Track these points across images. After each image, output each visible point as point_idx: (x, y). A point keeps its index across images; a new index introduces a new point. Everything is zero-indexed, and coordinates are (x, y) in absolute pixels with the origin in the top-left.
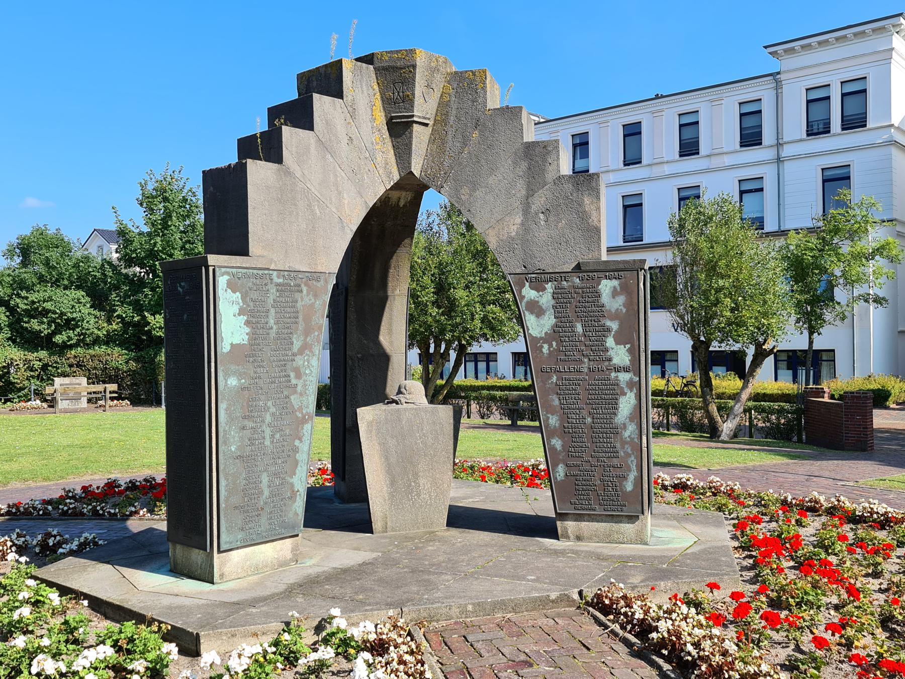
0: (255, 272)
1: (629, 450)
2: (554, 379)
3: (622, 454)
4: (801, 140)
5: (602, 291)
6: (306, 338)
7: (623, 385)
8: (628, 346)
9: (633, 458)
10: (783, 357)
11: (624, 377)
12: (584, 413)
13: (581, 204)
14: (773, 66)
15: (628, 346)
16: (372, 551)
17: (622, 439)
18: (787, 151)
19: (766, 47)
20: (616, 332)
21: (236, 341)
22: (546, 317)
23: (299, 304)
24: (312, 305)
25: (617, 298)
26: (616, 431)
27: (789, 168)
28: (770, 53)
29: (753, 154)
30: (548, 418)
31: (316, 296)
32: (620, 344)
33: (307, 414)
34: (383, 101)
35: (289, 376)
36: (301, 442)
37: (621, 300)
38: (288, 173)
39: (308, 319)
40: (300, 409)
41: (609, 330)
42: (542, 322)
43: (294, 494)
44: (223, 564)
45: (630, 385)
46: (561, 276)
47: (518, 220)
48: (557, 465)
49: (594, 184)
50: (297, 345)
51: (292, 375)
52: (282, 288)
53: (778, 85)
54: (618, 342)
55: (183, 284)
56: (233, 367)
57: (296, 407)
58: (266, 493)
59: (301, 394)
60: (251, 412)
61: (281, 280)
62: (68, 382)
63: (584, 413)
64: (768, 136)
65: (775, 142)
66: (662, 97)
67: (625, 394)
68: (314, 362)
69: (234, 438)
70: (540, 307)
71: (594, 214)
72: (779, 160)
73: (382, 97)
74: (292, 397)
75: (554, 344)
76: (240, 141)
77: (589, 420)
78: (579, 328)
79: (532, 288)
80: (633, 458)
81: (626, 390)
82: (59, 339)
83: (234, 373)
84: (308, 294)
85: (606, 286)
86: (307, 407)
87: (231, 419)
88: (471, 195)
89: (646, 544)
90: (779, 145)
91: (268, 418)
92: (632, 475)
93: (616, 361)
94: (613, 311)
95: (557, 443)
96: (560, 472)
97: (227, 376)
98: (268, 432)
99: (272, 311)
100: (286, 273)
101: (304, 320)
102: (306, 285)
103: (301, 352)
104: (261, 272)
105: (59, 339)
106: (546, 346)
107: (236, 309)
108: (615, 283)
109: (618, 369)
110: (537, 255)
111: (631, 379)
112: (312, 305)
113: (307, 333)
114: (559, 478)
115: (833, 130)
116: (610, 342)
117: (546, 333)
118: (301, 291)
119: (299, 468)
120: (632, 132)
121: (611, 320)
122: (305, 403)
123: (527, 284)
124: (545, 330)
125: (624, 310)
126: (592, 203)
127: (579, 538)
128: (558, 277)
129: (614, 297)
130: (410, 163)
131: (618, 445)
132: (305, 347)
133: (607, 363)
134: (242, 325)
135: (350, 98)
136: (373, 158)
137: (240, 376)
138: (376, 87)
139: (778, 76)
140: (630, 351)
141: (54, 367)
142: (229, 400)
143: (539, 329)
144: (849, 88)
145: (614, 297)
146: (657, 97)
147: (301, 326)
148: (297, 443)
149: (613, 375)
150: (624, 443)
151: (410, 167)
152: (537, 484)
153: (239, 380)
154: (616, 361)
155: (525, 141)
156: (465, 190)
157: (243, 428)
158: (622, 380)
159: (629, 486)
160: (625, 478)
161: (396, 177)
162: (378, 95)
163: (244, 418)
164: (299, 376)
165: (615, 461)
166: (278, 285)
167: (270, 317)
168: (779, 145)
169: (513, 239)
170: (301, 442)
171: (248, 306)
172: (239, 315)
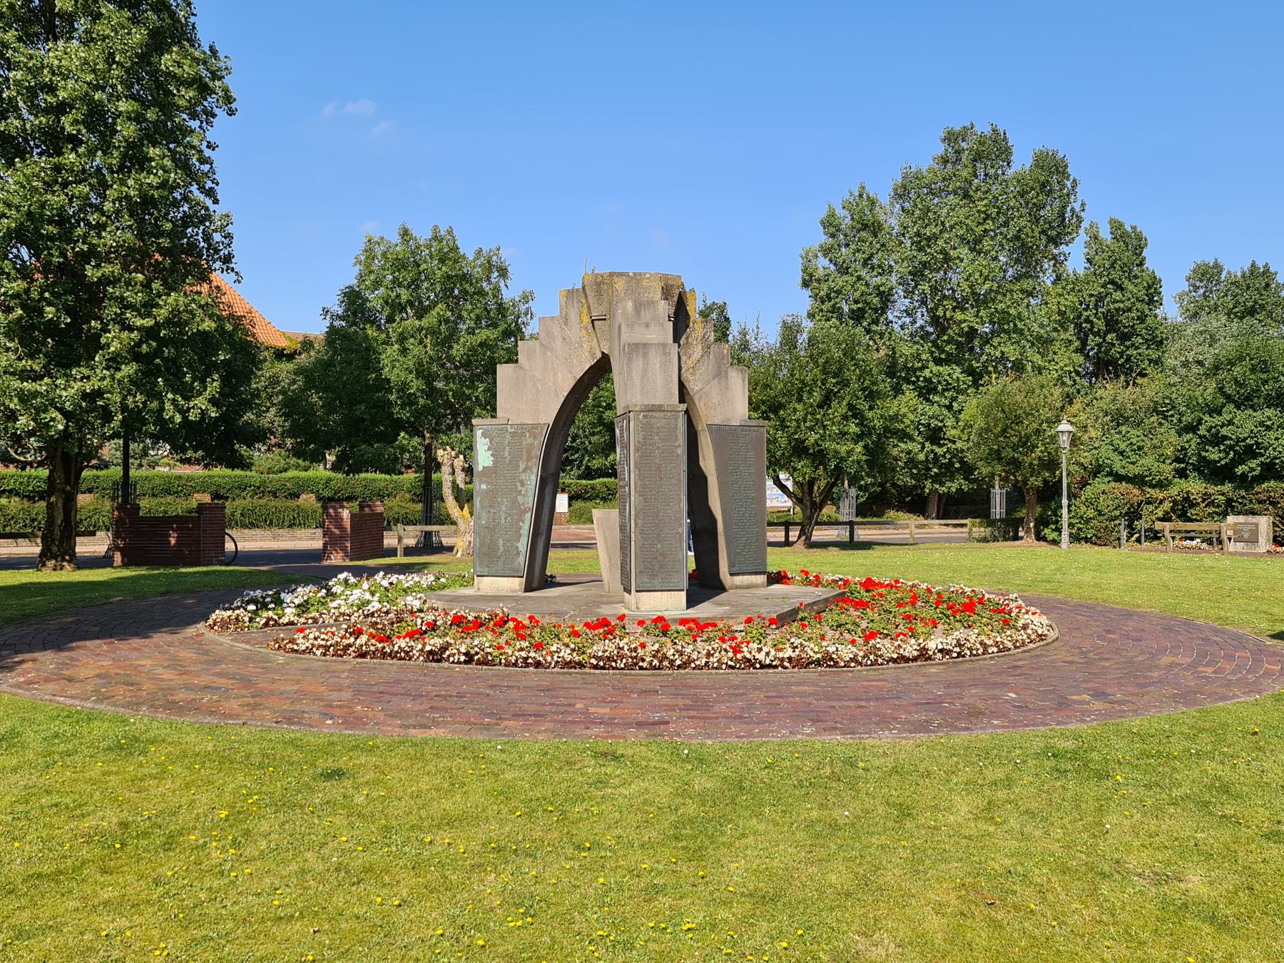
31: (535, 438)
38: (521, 368)
39: (529, 452)
40: (523, 504)
43: (518, 553)
44: (479, 583)
50: (522, 467)
52: (513, 435)
62: (1242, 521)
68: (533, 477)
82: (1240, 470)
83: (485, 482)
87: (482, 507)
91: (504, 508)
97: (480, 483)
98: (503, 516)
103: (524, 471)
105: (1240, 470)
107: (486, 447)
113: (528, 459)
137: (488, 484)
141: (1240, 503)
152: (1046, 607)
164: (523, 485)
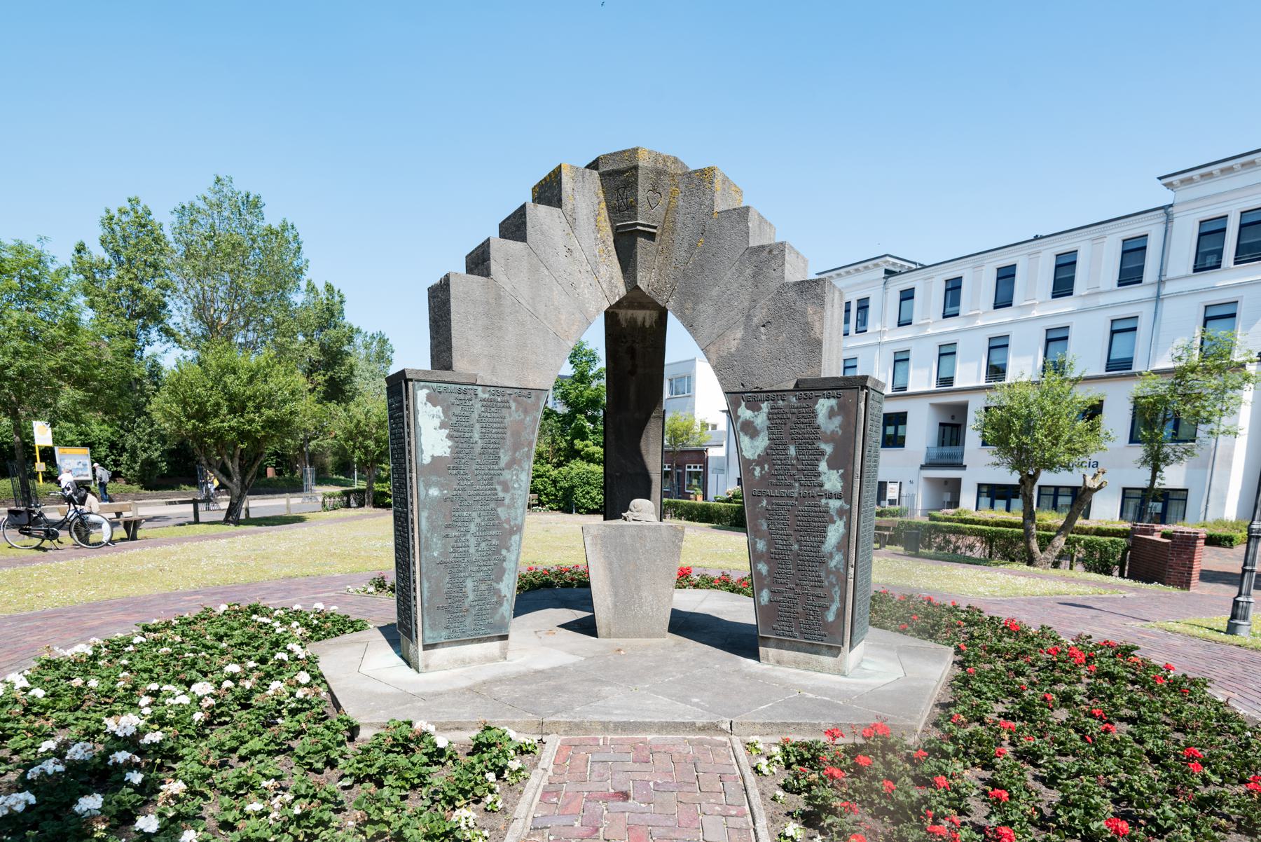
0: (458, 386)
1: (834, 581)
2: (764, 503)
3: (827, 584)
4: (1186, 277)
5: (819, 411)
6: (515, 452)
7: (833, 512)
8: (841, 471)
10: (985, 489)
11: (835, 504)
12: (792, 540)
13: (804, 315)
14: (1166, 197)
15: (841, 471)
16: (572, 653)
18: (1168, 289)
19: (1160, 178)
20: (830, 456)
22: (760, 439)
23: (507, 420)
24: (522, 422)
25: (833, 419)
26: (822, 561)
27: (1168, 306)
28: (1165, 185)
29: (1133, 292)
30: (756, 543)
31: (526, 412)
32: (833, 469)
34: (608, 210)
36: (509, 551)
37: (837, 421)
39: (517, 434)
41: (823, 454)
42: (756, 443)
45: (841, 513)
47: (739, 334)
48: (762, 590)
49: (819, 291)
50: (504, 459)
51: (499, 488)
53: (1169, 220)
54: (831, 467)
56: (434, 478)
57: (503, 518)
58: (471, 597)
59: (509, 507)
60: (452, 523)
61: (487, 396)
63: (792, 540)
64: (1150, 273)
65: (1156, 279)
66: (1042, 237)
67: (834, 522)
69: (436, 544)
70: (755, 428)
71: (817, 325)
72: (1158, 298)
73: (607, 206)
74: (499, 510)
77: (796, 547)
78: (792, 451)
79: (748, 408)
81: (835, 518)
83: (436, 484)
85: (824, 406)
86: (515, 519)
88: (694, 310)
89: (843, 675)
90: (1161, 282)
91: (473, 528)
92: (834, 608)
93: (827, 486)
94: (828, 432)
95: (763, 568)
97: (428, 485)
98: (472, 542)
99: (477, 426)
101: (512, 435)
102: (515, 400)
103: (509, 466)
104: (463, 387)
106: (758, 469)
107: (437, 422)
108: (833, 402)
109: (830, 496)
110: (756, 372)
111: (841, 507)
113: (516, 447)
114: (763, 603)
115: (1224, 264)
116: (823, 466)
117: (759, 456)
119: (506, 576)
120: (1006, 276)
121: (826, 442)
122: (513, 515)
123: (743, 404)
124: (759, 451)
125: (840, 432)
126: (815, 313)
127: (779, 662)
128: (774, 395)
129: (830, 418)
130: (635, 277)
131: (823, 574)
133: (818, 489)
134: (444, 438)
135: (569, 207)
136: (595, 273)
137: (442, 487)
138: (602, 196)
139: (1170, 209)
140: (843, 477)
142: (429, 509)
145: (830, 418)
146: (1036, 238)
147: (509, 441)
148: (504, 552)
149: (824, 501)
150: (829, 572)
151: (636, 281)
153: (441, 491)
154: (827, 486)
155: (753, 243)
156: (689, 305)
157: (447, 536)
158: (832, 507)
159: (831, 617)
160: (827, 608)
161: (622, 291)
162: (603, 205)
165: (819, 592)
167: (475, 431)
168: (1161, 282)
169: (732, 355)
170: (509, 551)
172: (440, 428)
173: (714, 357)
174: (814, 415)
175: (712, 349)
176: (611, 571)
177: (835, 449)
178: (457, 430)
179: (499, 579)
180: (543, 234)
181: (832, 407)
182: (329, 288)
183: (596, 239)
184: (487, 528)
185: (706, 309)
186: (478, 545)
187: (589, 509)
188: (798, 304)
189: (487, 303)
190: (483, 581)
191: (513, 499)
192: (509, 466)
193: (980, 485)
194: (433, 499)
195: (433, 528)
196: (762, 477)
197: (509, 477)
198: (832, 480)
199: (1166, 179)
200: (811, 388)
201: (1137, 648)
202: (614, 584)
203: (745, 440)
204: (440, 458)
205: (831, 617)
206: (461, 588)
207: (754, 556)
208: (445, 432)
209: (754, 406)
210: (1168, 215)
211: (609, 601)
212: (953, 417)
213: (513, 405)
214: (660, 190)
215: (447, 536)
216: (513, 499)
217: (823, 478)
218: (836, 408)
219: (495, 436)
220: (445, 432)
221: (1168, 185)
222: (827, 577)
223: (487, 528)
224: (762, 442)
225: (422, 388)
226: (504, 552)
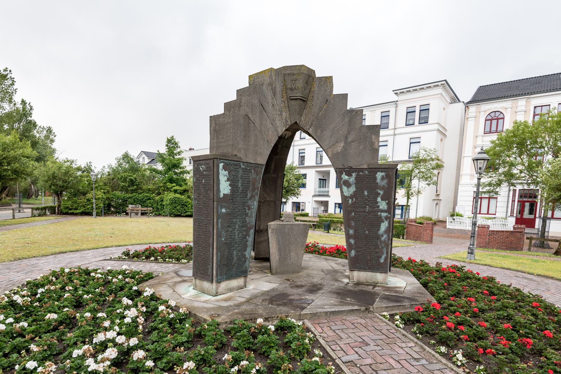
0: (234, 162)
2: (353, 214)
5: (377, 177)
8: (387, 201)
9: (385, 249)
11: (384, 214)
13: (371, 138)
14: (395, 98)
15: (387, 201)
17: (381, 241)
18: (397, 131)
19: (393, 91)
21: (226, 193)
22: (351, 188)
23: (251, 177)
24: (255, 179)
26: (379, 237)
31: (257, 174)
33: (252, 225)
35: (245, 209)
37: (385, 181)
39: (254, 184)
40: (249, 223)
42: (349, 190)
45: (387, 218)
46: (362, 170)
47: (342, 144)
48: (351, 250)
50: (249, 195)
51: (247, 208)
52: (245, 170)
54: (382, 200)
55: (202, 166)
56: (224, 204)
57: (248, 222)
58: (235, 259)
59: (250, 217)
61: (244, 167)
64: (391, 126)
65: (393, 128)
67: (384, 222)
74: (246, 218)
75: (354, 199)
76: (237, 91)
77: (367, 232)
78: (366, 193)
79: (346, 175)
80: (385, 249)
81: (384, 220)
84: (254, 174)
86: (252, 222)
88: (321, 133)
91: (237, 227)
92: (383, 257)
93: (381, 207)
94: (382, 186)
95: (352, 241)
96: (353, 253)
98: (237, 233)
99: (240, 180)
100: (246, 164)
102: (254, 169)
103: (250, 199)
104: (236, 163)
107: (226, 178)
108: (383, 174)
111: (387, 215)
112: (255, 179)
114: (352, 256)
116: (379, 199)
117: (351, 195)
118: (251, 172)
121: (381, 190)
123: (344, 173)
124: (351, 193)
125: (386, 186)
129: (382, 180)
132: (252, 196)
136: (281, 114)
140: (388, 204)
142: (222, 218)
143: (348, 193)
144: (423, 108)
145: (382, 180)
150: (381, 242)
153: (226, 210)
154: (381, 207)
156: (319, 131)
159: (382, 261)
160: (381, 257)
163: (228, 226)
165: (377, 250)
166: (243, 169)
171: (231, 177)
172: (227, 181)
173: (330, 154)
174: (375, 178)
175: (330, 150)
176: (279, 245)
177: (384, 193)
178: (232, 181)
179: (245, 250)
180: (265, 97)
181: (383, 176)
182: (23, 102)
183: (282, 101)
184: (242, 227)
185: (327, 133)
186: (238, 235)
187: (175, 215)
188: (368, 134)
189: (245, 126)
190: (239, 251)
191: (251, 213)
192: (250, 199)
193: (336, 204)
194: (224, 214)
195: (223, 227)
196: (352, 203)
197: (250, 203)
198: (383, 205)
199: (397, 92)
200: (374, 170)
201: (465, 267)
202: (280, 250)
203: (345, 188)
204: (226, 194)
205: (382, 261)
206: (232, 255)
207: (348, 237)
208: (229, 183)
209: (349, 174)
210: (396, 104)
211: (277, 258)
212: (323, 176)
213: (253, 171)
214: (309, 83)
215: (227, 231)
216: (251, 213)
217: (379, 204)
218: (385, 176)
219: (246, 185)
220: (229, 183)
221: (396, 94)
222: (381, 244)
223: (242, 227)
224: (353, 189)
225: (221, 163)
226: (247, 237)
